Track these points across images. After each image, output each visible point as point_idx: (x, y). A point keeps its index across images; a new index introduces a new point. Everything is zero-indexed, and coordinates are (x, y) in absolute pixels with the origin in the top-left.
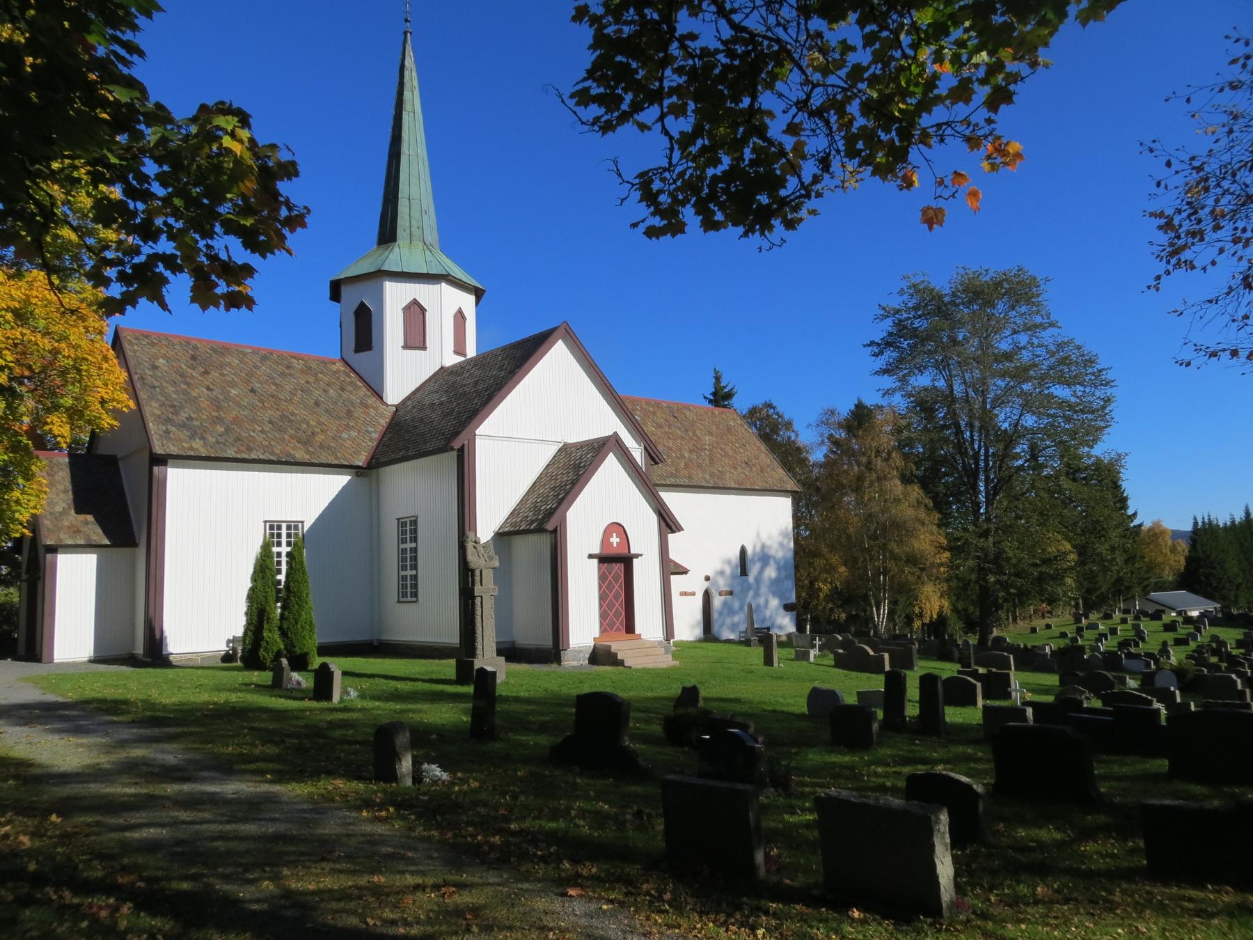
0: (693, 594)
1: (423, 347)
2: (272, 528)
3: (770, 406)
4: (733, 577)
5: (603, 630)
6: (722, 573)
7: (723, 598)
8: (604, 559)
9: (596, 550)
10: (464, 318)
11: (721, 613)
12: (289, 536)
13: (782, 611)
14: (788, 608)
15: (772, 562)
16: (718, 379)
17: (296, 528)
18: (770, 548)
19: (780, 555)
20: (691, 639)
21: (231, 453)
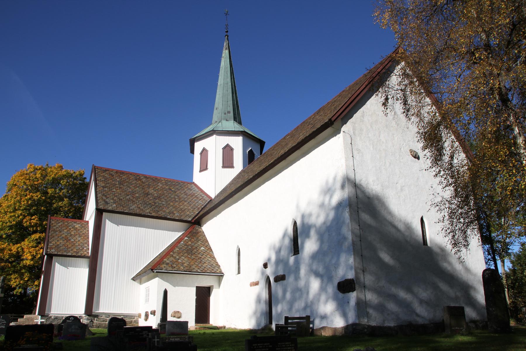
18: (310, 215)
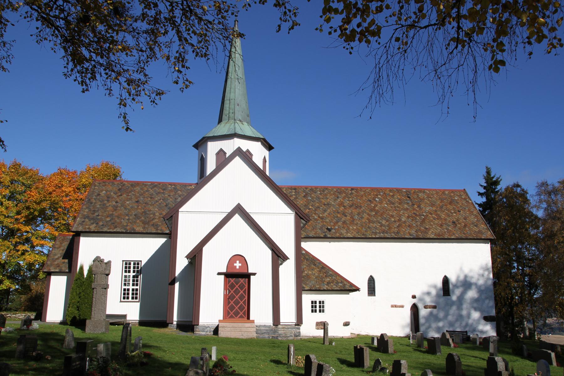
0: (402, 307)
2: (126, 264)
3: (518, 186)
4: (438, 295)
5: (225, 317)
6: (428, 293)
7: (429, 310)
8: (228, 275)
9: (224, 270)
12: (134, 268)
13: (483, 322)
14: (487, 319)
15: (473, 287)
16: (488, 173)
17: (138, 264)
19: (481, 282)
20: (402, 335)
21: (105, 229)
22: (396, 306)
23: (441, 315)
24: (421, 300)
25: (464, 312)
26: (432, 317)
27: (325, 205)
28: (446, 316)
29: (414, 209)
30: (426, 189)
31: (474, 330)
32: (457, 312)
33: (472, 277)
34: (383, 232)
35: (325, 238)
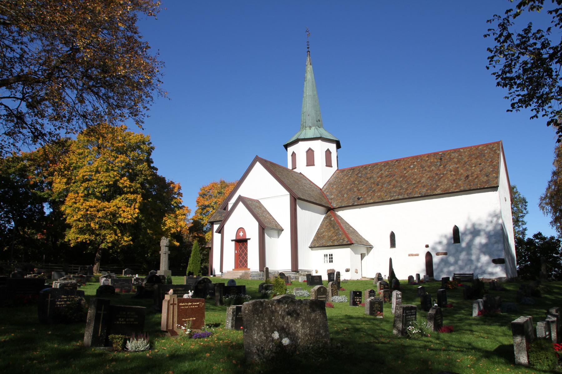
0: (417, 255)
1: (314, 165)
4: (449, 244)
6: (440, 243)
7: (440, 256)
9: (235, 239)
10: (330, 153)
11: (439, 265)
13: (493, 265)
14: (497, 262)
15: (482, 233)
22: (412, 255)
23: (451, 259)
24: (434, 249)
25: (474, 257)
26: (444, 262)
27: (367, 179)
28: (456, 262)
29: (439, 170)
30: (461, 148)
31: (484, 273)
32: (466, 257)
33: (480, 225)
34: (400, 194)
35: (353, 206)
